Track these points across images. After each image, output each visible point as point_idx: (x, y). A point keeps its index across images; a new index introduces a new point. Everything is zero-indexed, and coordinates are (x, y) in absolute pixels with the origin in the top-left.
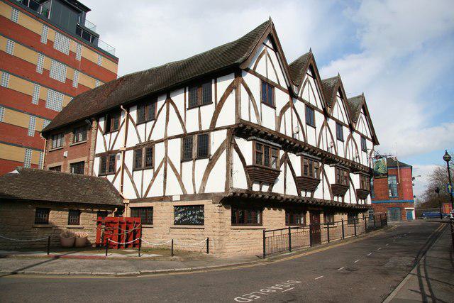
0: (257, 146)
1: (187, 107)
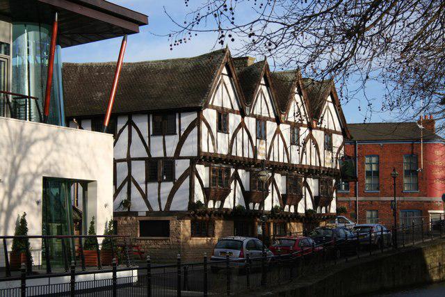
0: (212, 171)
1: (151, 133)
